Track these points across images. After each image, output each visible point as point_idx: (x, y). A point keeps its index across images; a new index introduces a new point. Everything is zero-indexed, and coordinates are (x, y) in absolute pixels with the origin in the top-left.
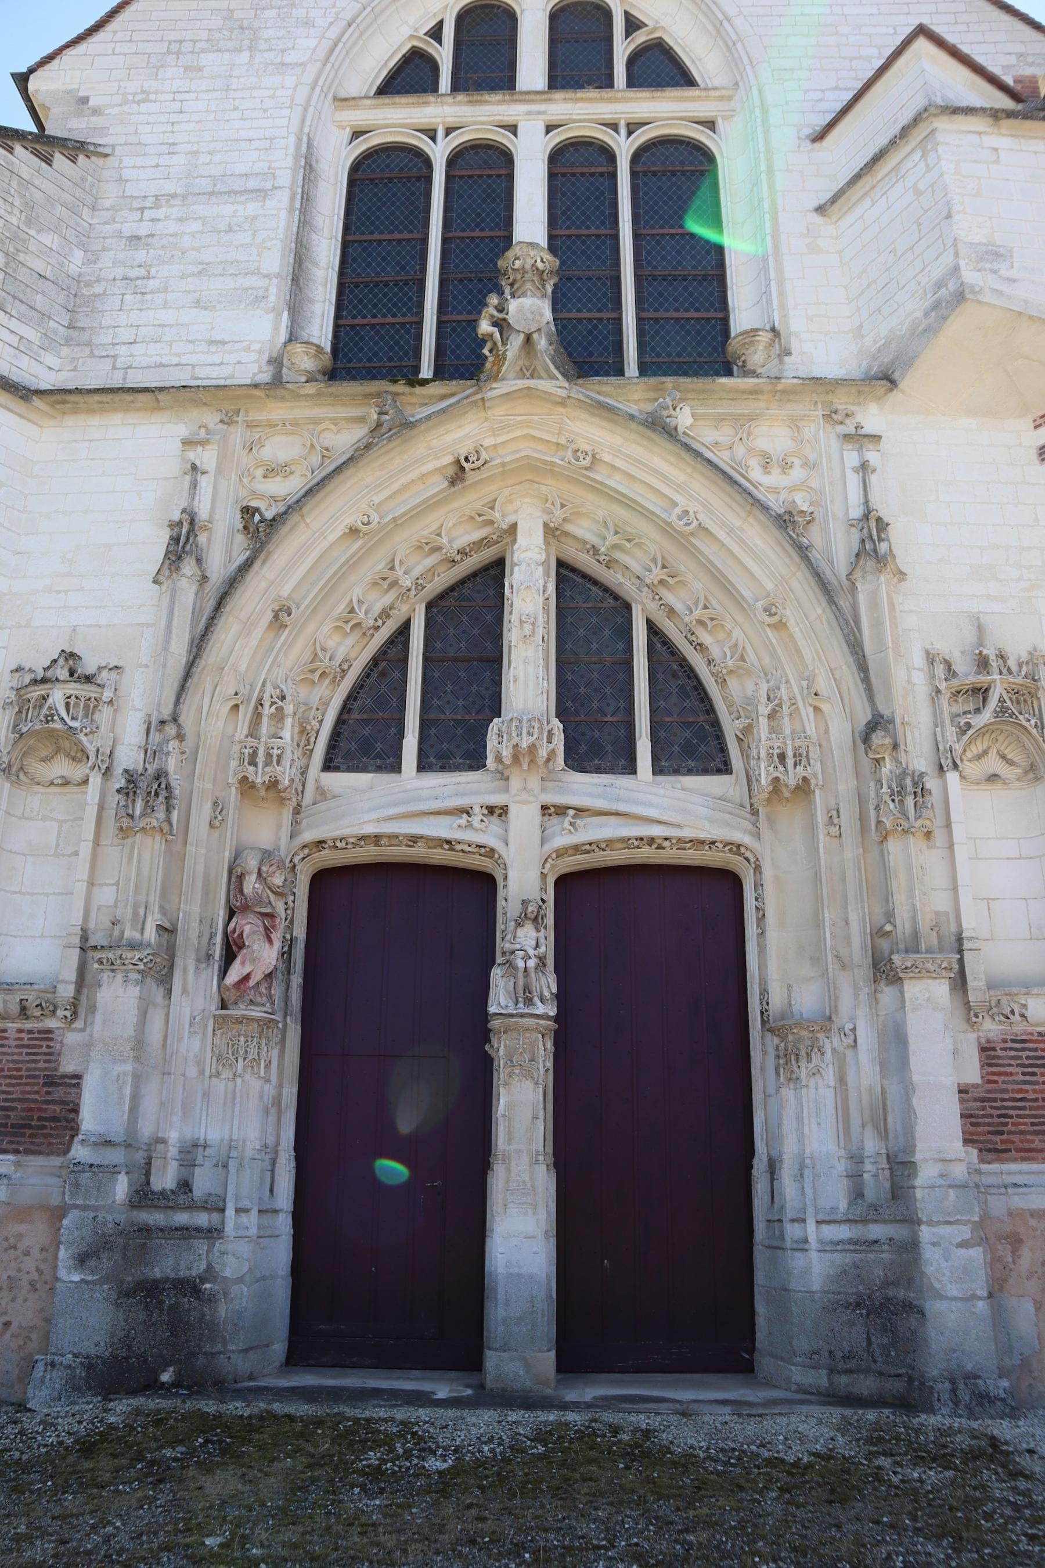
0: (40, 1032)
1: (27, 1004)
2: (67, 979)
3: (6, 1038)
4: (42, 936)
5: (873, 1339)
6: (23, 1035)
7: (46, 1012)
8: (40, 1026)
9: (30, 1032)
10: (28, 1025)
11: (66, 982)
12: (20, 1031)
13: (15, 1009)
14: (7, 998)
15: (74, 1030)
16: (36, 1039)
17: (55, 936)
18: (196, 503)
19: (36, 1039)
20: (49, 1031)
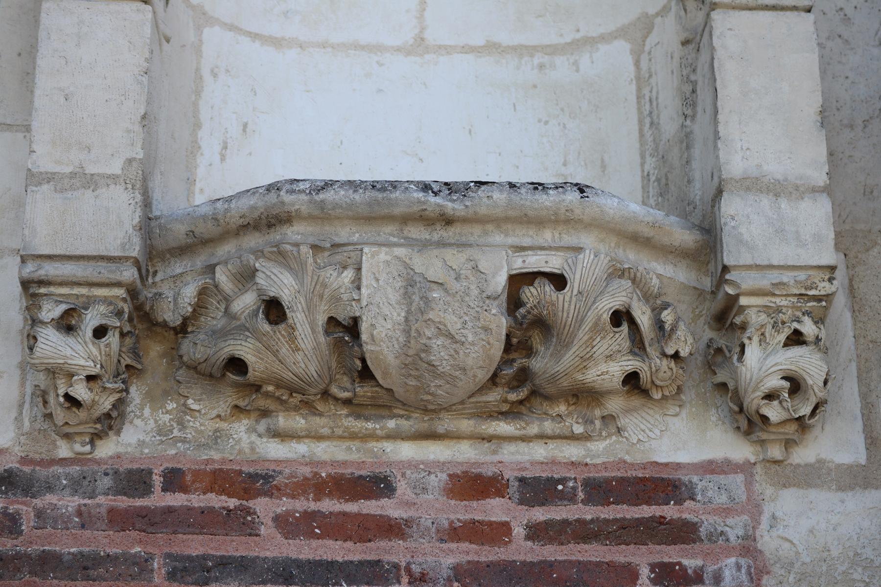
0: (600, 490)
1: (564, 303)
2: (775, 168)
3: (392, 529)
4: (419, 46)
5: (150, 268)
6: (495, 509)
7: (654, 367)
8: (599, 453)
9: (539, 489)
10: (525, 451)
11: (776, 189)
12: (473, 485)
13: (475, 336)
14: (430, 265)
15: (811, 477)
16: (584, 532)
17: (492, 48)
18: (116, 168)
19: (584, 532)
20: (662, 485)
